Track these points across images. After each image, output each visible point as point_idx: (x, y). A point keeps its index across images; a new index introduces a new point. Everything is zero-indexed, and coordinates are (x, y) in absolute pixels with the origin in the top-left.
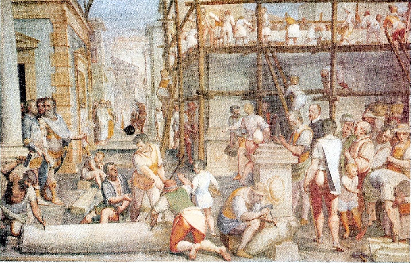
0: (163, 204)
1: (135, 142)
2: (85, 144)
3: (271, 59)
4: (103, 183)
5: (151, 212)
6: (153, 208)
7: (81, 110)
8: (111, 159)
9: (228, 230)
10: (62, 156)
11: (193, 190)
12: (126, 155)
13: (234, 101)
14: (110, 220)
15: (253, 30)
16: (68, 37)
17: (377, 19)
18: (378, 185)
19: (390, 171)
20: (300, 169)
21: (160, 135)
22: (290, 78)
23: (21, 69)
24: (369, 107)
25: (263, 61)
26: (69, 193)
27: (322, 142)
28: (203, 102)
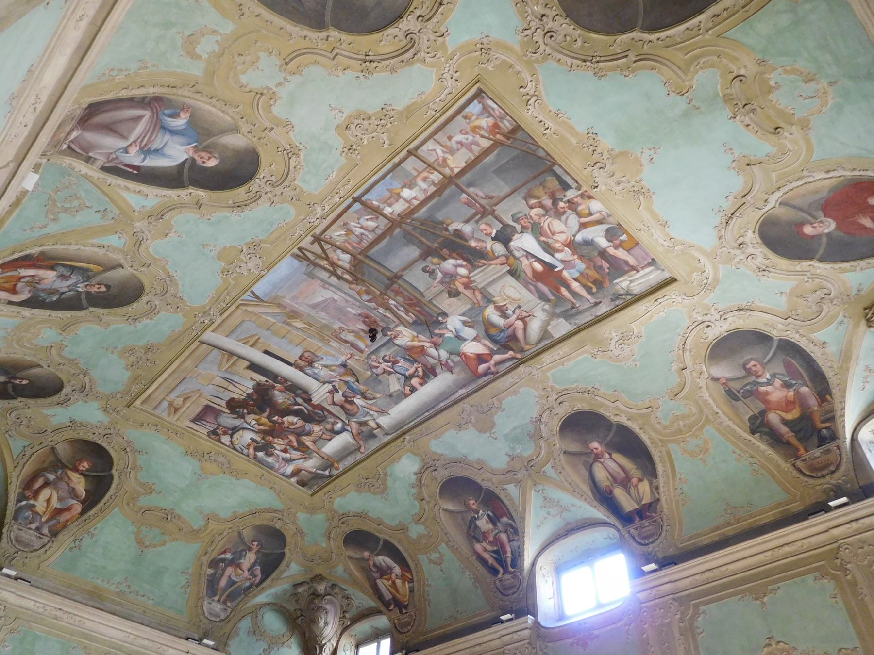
0: (444, 354)
8: (382, 354)
13: (421, 265)
14: (421, 384)
15: (377, 218)
18: (589, 243)
21: (396, 320)
22: (442, 223)
23: (266, 352)
24: (528, 197)
26: (380, 387)
28: (400, 282)
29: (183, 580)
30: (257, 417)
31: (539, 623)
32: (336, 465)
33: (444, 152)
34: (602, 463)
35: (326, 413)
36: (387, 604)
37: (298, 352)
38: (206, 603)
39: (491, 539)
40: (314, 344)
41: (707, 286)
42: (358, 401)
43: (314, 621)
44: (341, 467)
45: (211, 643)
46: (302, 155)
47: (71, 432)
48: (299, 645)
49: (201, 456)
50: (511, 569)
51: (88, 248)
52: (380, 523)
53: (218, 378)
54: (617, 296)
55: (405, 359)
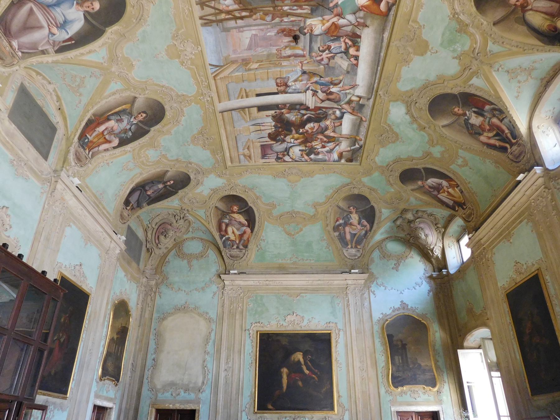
5: (355, 26)
6: (353, 24)
7: (283, 64)
10: (313, 74)
12: (314, 38)
14: (358, 50)
16: (236, 74)
21: (300, 18)
23: (258, 95)
26: (337, 71)
29: (324, 244)
30: (291, 136)
31: (547, 169)
32: (358, 138)
34: (531, 10)
35: (324, 110)
36: (453, 208)
38: (344, 251)
39: (488, 127)
40: (275, 71)
42: (334, 89)
43: (417, 238)
45: (357, 271)
47: (216, 195)
48: (419, 254)
49: (283, 175)
50: (514, 141)
51: (110, 98)
52: (412, 159)
53: (251, 127)
55: (333, 41)
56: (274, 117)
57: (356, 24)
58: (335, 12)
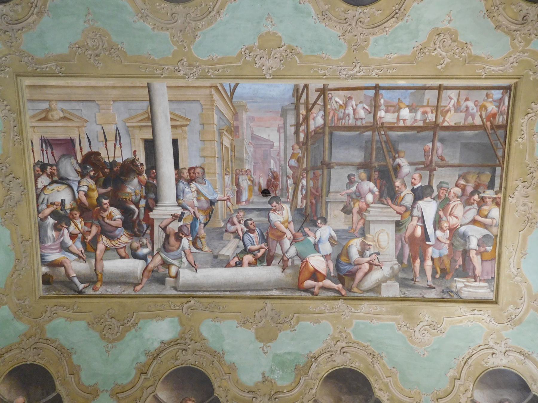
0: (292, 251)
1: (270, 203)
2: (229, 204)
3: (384, 136)
4: (243, 235)
5: (283, 258)
6: (284, 255)
7: (226, 177)
8: (250, 216)
9: (344, 272)
11: (317, 240)
12: (263, 213)
14: (250, 264)
15: (370, 113)
16: (216, 117)
17: (474, 104)
18: (465, 237)
19: (475, 227)
20: (402, 224)
21: (291, 197)
22: (397, 152)
23: (175, 142)
24: (463, 176)
25: (377, 138)
26: (216, 243)
27: (420, 203)
28: (326, 171)
30: (94, 187)
32: (98, 285)
33: (454, 105)
35: (148, 232)
37: (196, 162)
41: (514, 321)
44: (102, 290)
46: (400, 23)
52: (75, 371)
53: (114, 127)
54: (448, 291)
55: (261, 235)
56: (133, 162)
57: (285, 258)
58: (297, 234)
